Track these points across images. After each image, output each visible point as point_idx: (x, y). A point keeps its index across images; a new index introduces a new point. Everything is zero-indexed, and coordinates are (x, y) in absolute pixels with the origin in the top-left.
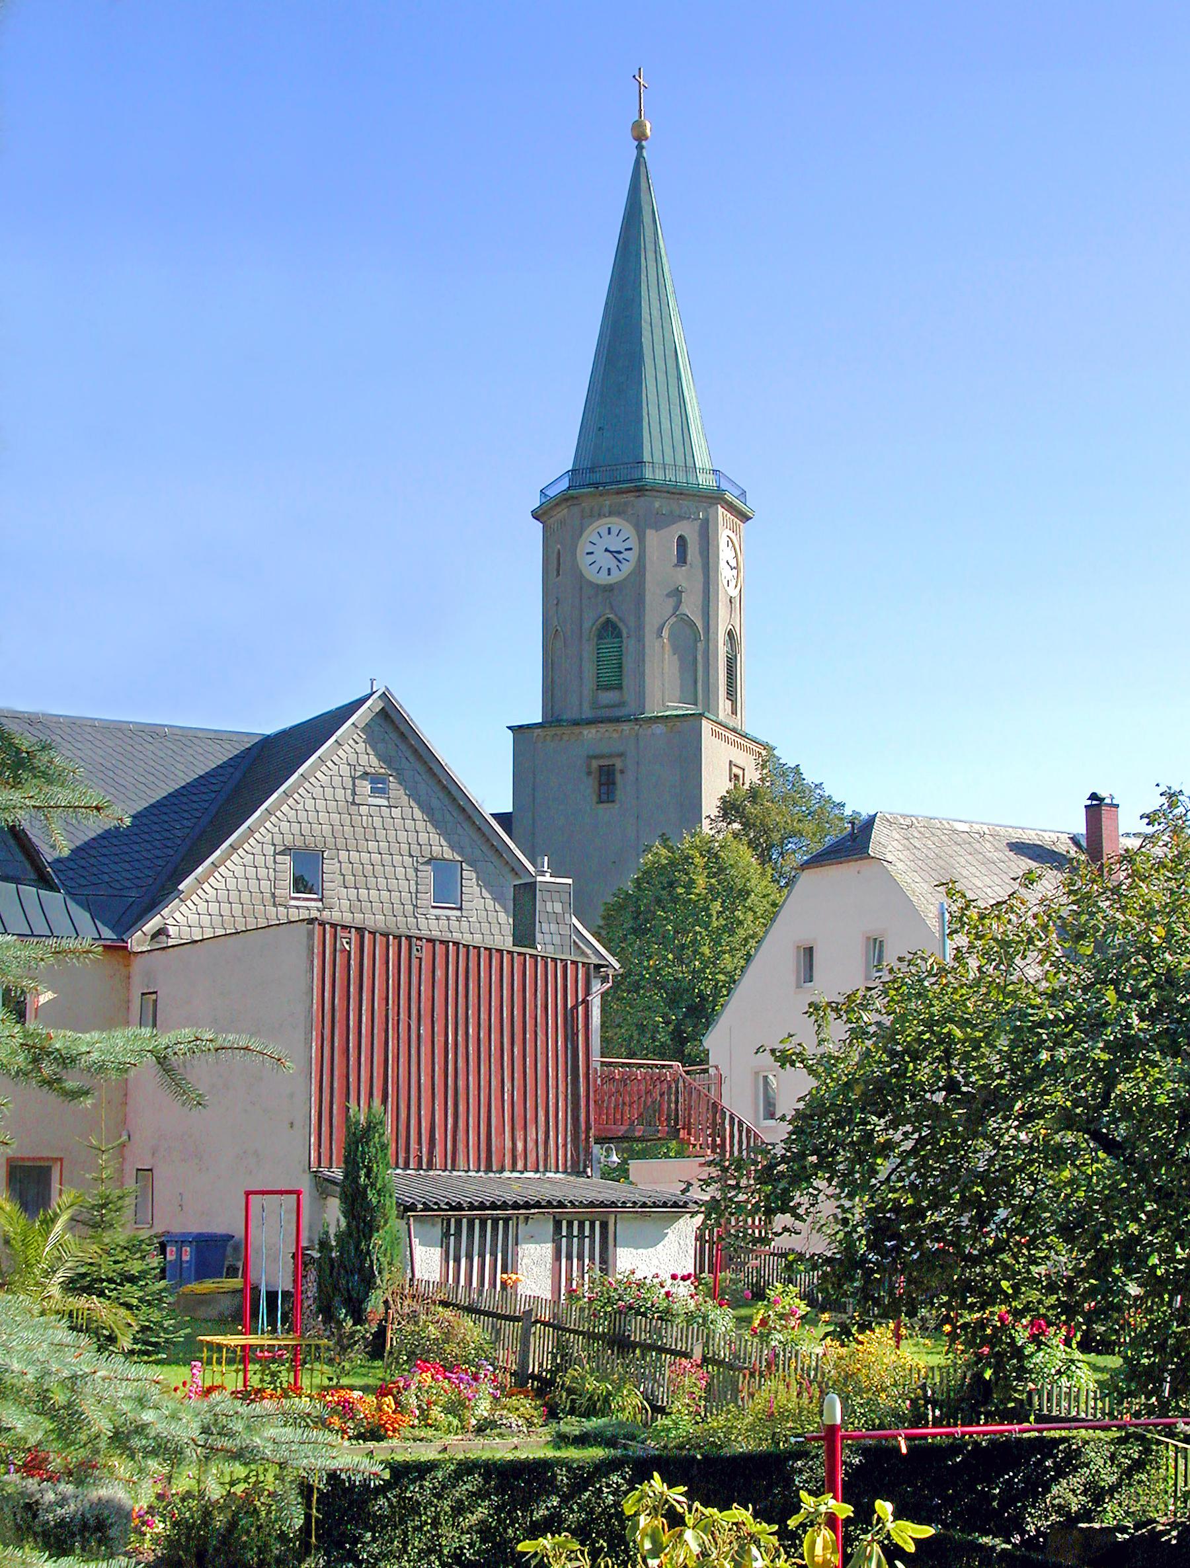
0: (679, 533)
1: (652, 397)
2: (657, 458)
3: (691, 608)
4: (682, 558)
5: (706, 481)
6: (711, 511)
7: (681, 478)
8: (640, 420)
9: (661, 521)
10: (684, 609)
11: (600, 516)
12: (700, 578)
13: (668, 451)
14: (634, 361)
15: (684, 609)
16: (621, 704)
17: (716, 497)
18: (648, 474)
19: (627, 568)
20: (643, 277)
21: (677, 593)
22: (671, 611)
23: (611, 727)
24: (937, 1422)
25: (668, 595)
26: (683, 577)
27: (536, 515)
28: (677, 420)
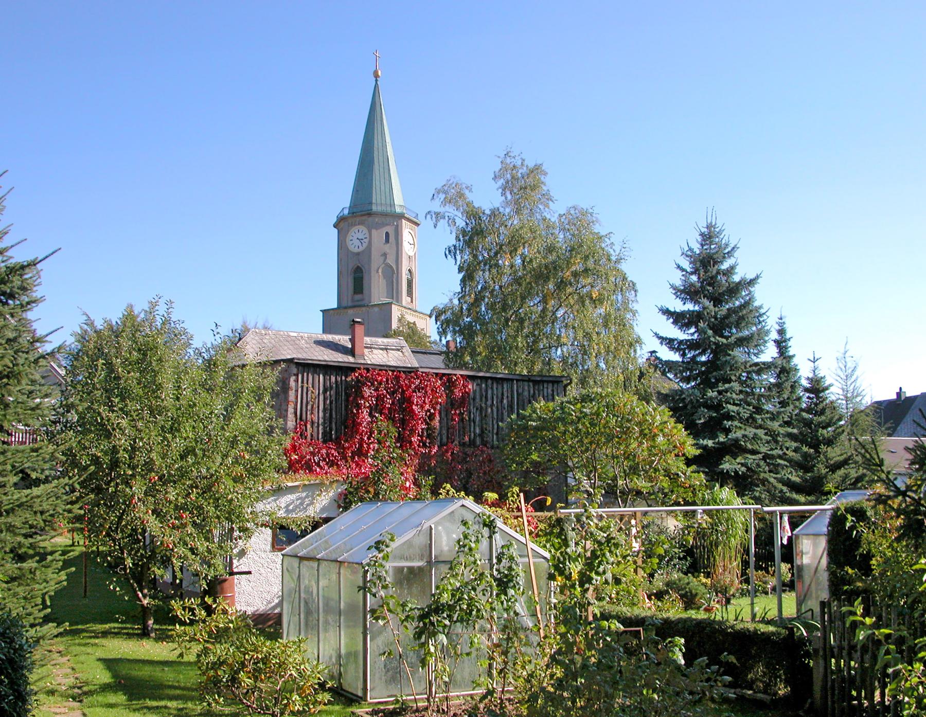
2: (379, 202)
3: (391, 261)
4: (387, 241)
5: (398, 210)
7: (389, 209)
8: (372, 188)
9: (378, 226)
10: (388, 261)
11: (355, 225)
13: (383, 198)
14: (372, 162)
15: (388, 261)
16: (362, 300)
17: (401, 216)
18: (374, 208)
19: (365, 245)
21: (385, 255)
23: (358, 309)
24: (286, 421)
26: (389, 249)
27: (335, 226)
28: (387, 186)
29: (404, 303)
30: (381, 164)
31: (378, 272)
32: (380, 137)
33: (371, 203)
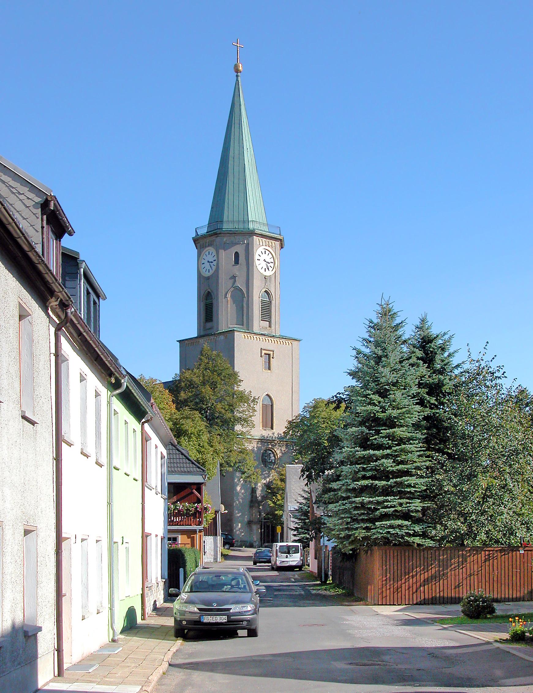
0: (235, 251)
1: (231, 190)
3: (240, 284)
4: (237, 262)
5: (251, 226)
6: (250, 239)
7: (241, 226)
8: (224, 202)
9: (225, 247)
11: (206, 247)
12: (245, 270)
17: (252, 233)
20: (232, 137)
21: (234, 277)
22: (231, 285)
25: (230, 279)
26: (239, 271)
29: (256, 329)
30: (236, 174)
31: (226, 297)
32: (236, 144)
33: (222, 222)
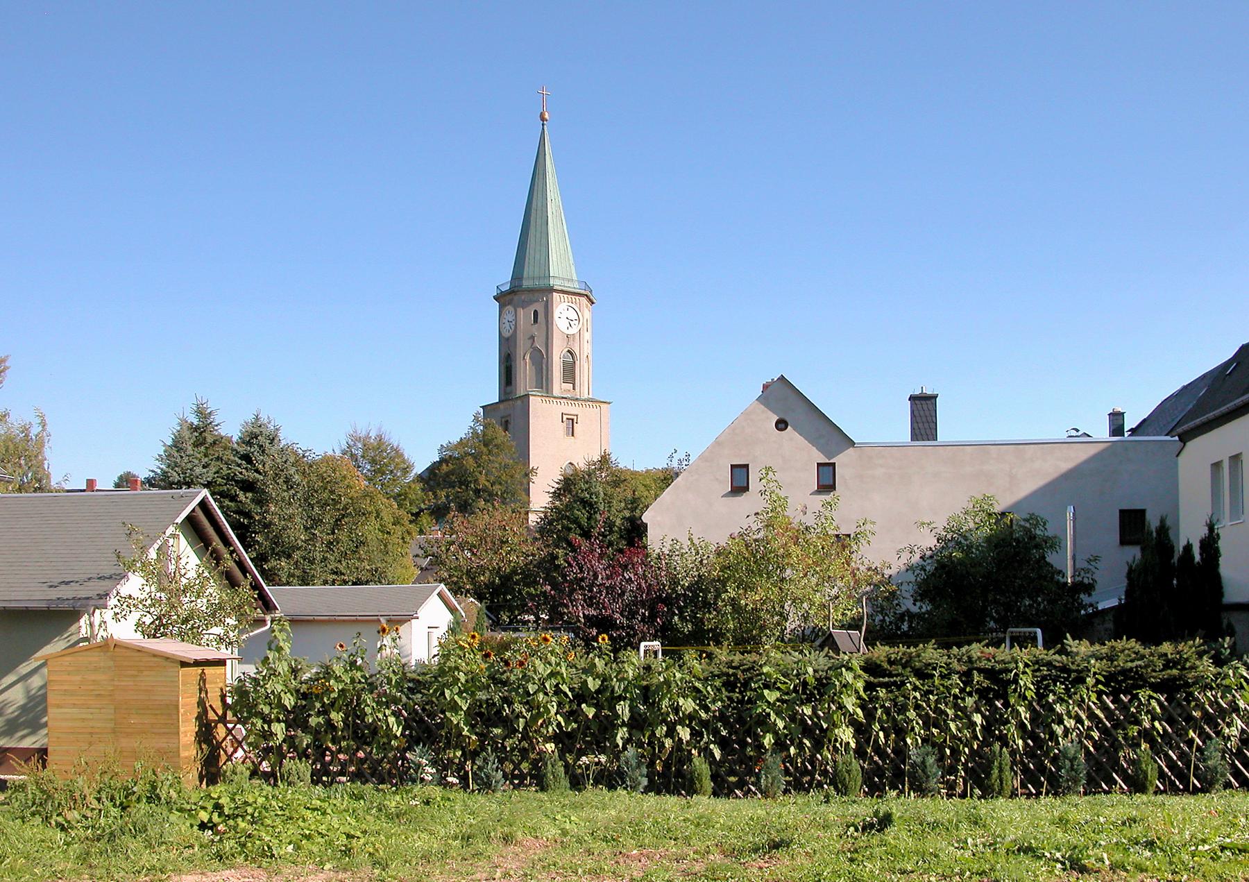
3: (539, 345)
9: (524, 305)
21: (532, 338)
26: (537, 331)
